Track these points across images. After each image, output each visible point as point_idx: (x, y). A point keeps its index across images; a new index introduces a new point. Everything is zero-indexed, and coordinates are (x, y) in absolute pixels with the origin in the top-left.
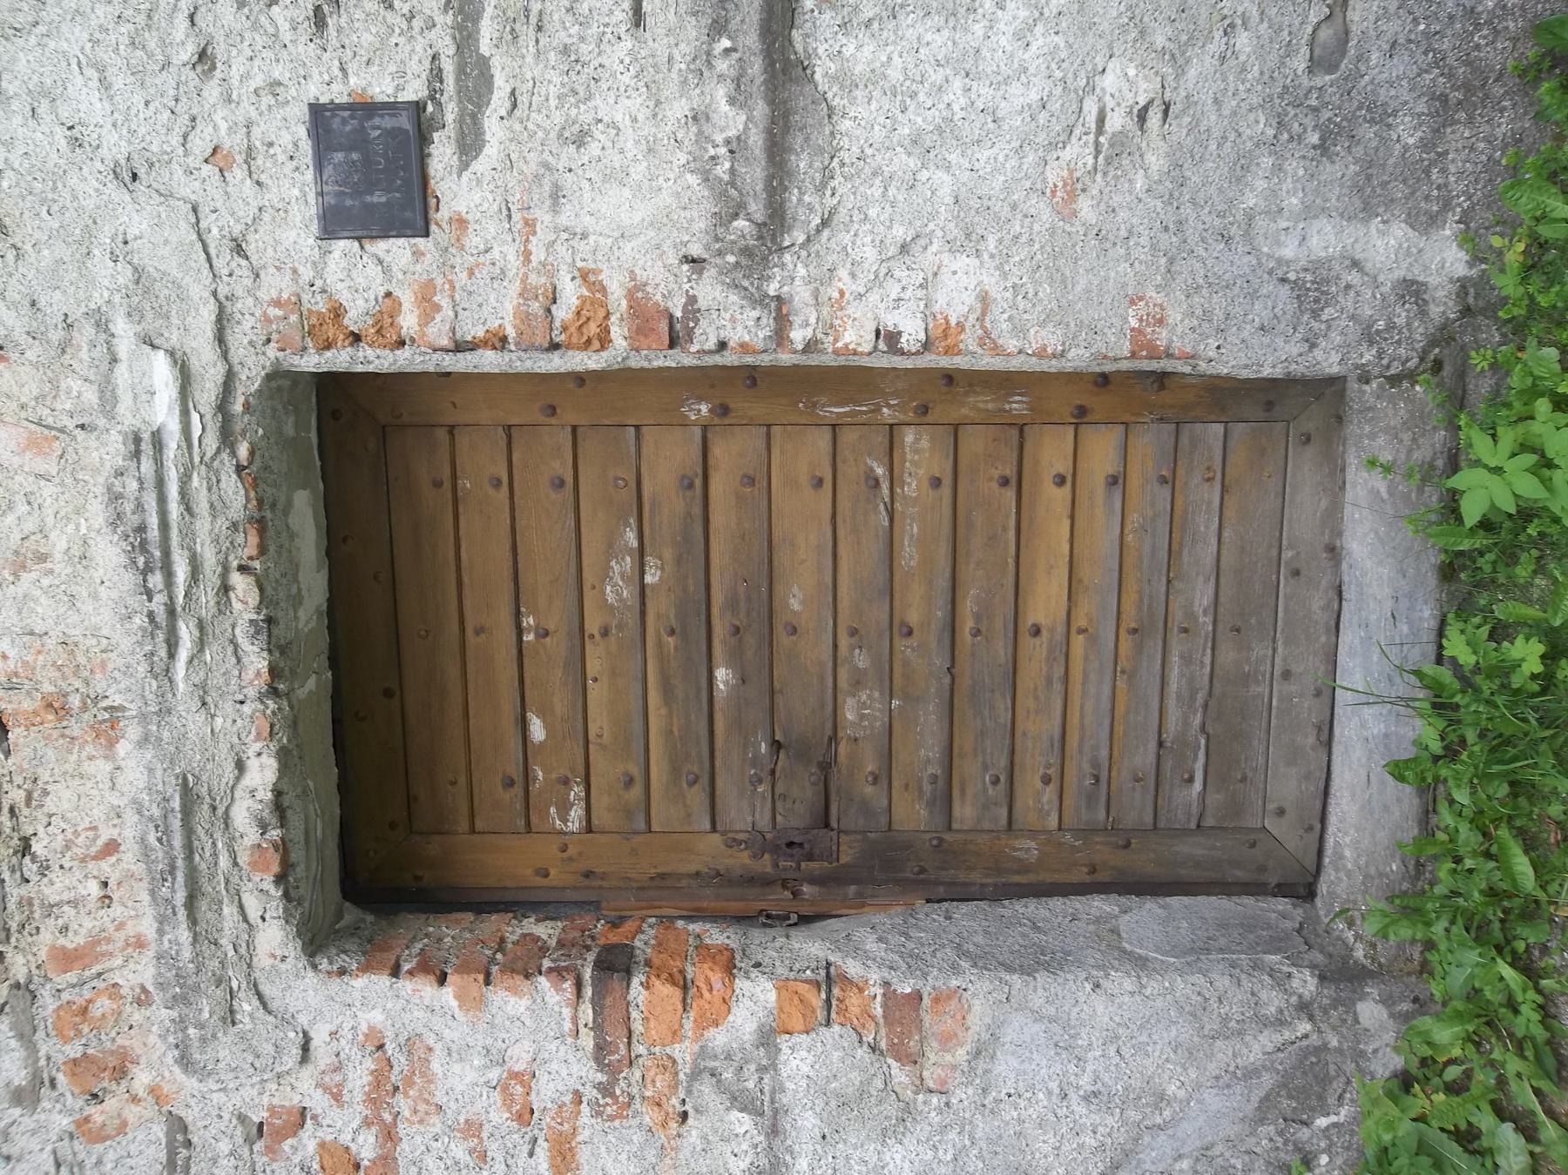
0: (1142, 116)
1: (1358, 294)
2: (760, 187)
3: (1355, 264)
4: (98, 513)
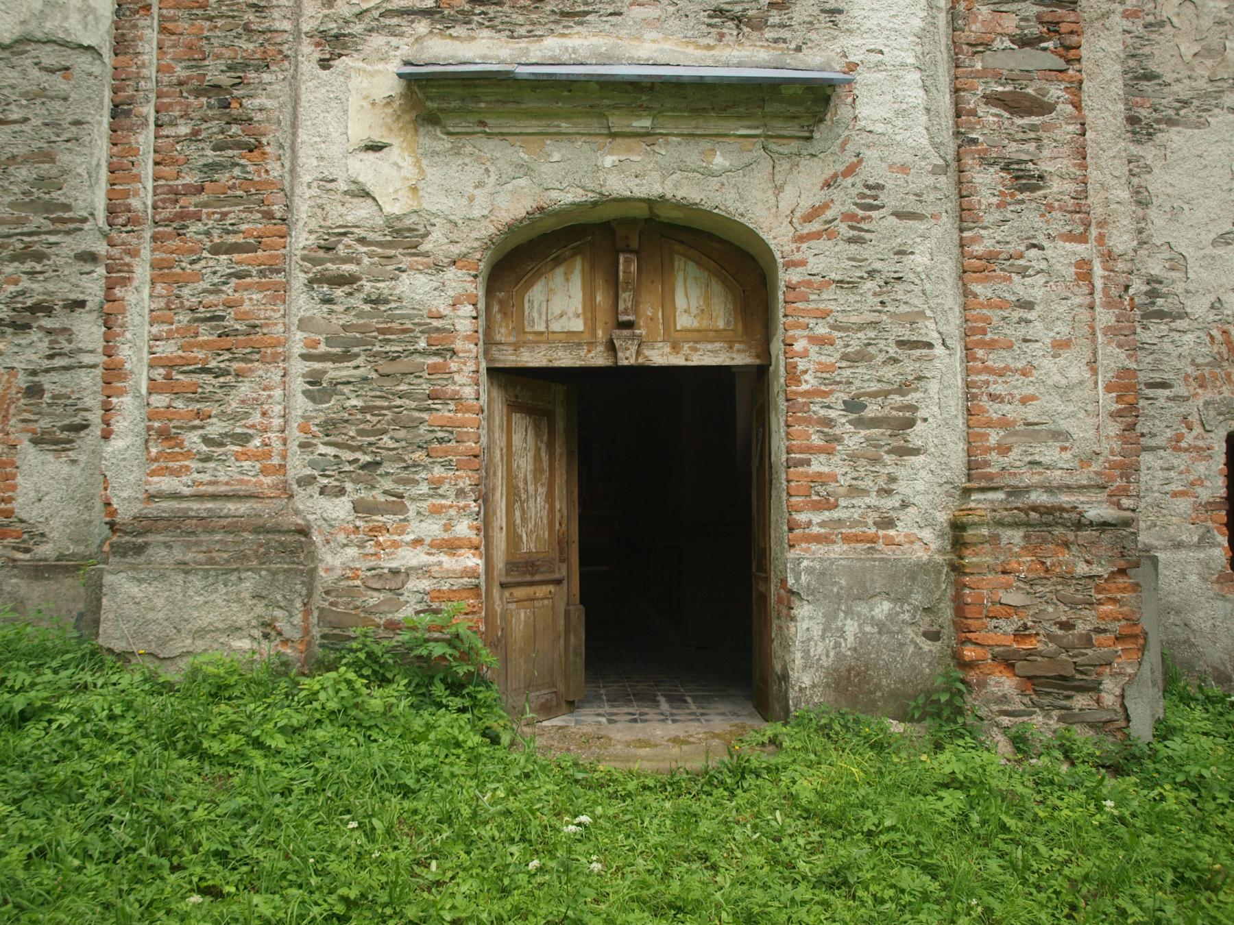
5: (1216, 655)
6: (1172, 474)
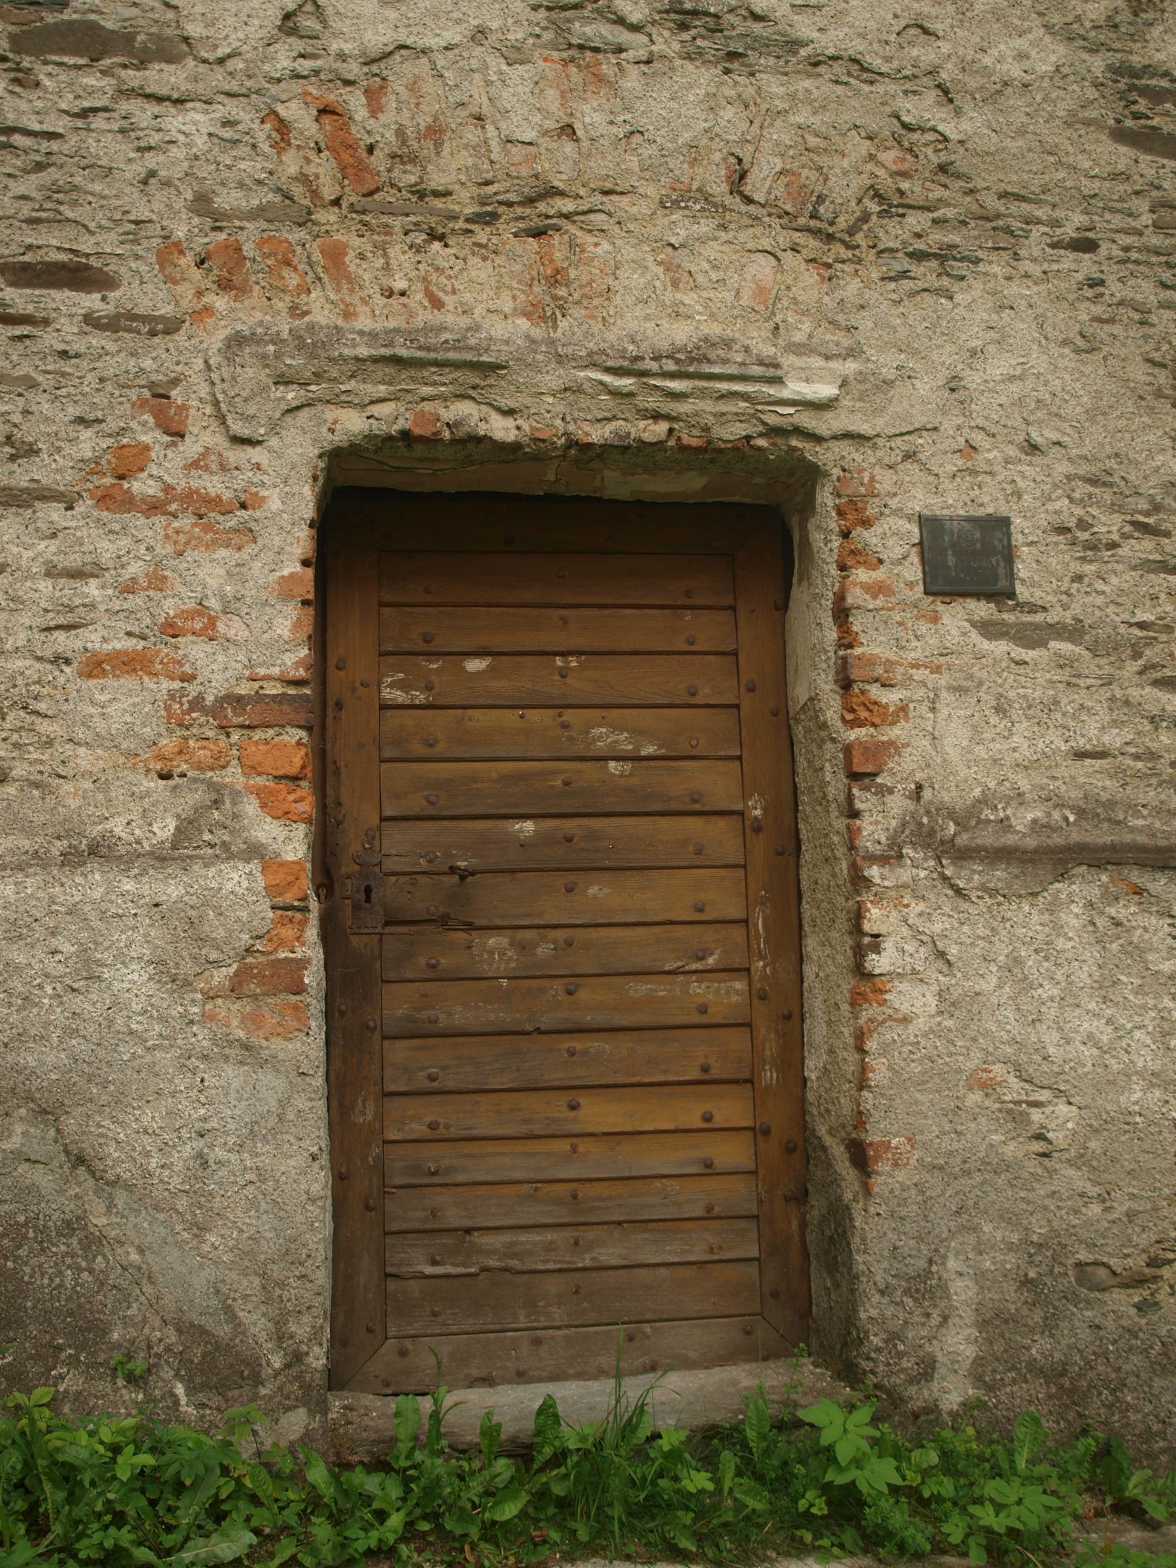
0: (1040, 1137)
1: (923, 1324)
2: (979, 841)
3: (945, 1318)
4: (714, 330)
5: (202, 1279)
6: (92, 589)
